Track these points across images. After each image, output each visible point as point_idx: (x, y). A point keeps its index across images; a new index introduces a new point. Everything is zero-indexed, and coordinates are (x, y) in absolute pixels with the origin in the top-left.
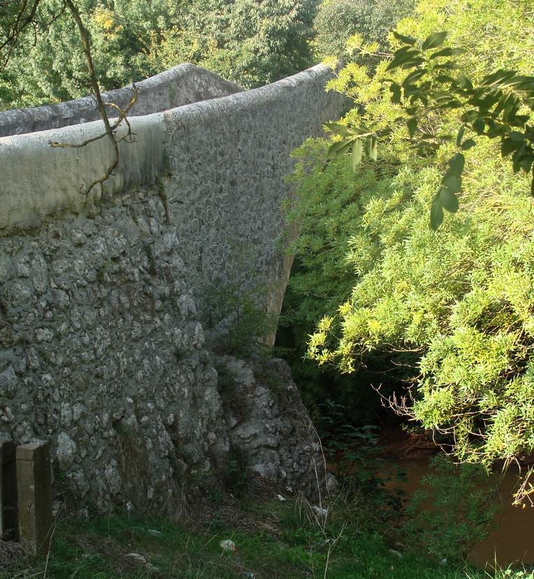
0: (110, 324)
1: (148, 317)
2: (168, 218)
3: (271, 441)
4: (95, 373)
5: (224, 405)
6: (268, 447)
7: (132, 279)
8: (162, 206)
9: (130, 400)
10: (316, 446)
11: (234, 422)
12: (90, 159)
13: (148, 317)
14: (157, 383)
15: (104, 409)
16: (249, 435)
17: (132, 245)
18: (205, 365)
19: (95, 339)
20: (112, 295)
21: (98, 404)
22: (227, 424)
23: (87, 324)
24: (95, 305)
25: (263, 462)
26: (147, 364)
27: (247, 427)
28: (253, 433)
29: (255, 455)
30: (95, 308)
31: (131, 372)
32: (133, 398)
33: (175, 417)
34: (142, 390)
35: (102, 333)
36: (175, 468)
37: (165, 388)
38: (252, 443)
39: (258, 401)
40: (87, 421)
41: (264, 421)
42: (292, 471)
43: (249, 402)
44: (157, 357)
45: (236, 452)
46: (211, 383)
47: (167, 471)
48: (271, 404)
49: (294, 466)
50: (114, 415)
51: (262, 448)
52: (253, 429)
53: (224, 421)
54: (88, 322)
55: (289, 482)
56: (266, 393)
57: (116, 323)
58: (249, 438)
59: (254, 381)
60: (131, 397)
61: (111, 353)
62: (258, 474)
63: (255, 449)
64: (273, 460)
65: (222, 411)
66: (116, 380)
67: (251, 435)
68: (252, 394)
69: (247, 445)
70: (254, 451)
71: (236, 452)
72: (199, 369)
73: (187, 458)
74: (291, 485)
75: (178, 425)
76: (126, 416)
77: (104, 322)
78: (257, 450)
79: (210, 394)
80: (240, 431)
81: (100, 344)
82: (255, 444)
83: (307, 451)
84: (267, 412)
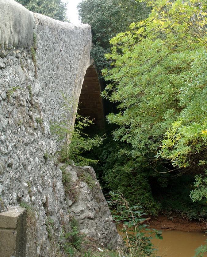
0: (14, 130)
1: (31, 131)
2: (36, 73)
3: (91, 214)
4: (8, 163)
5: (65, 193)
6: (90, 218)
7: (23, 104)
8: (33, 65)
9: (26, 185)
10: (111, 218)
11: (70, 202)
12: (4, 16)
13: (31, 131)
14: (37, 175)
15: (13, 190)
16: (79, 211)
17: (22, 83)
18: (56, 166)
19: (7, 139)
20: (14, 112)
21: (11, 185)
22: (67, 204)
23: (3, 127)
24: (6, 115)
25: (87, 227)
26: (33, 161)
27: (77, 206)
28: (81, 209)
29: (82, 223)
30: (6, 117)
31: (26, 165)
32: (27, 183)
33: (47, 198)
34: (31, 178)
35: (10, 135)
36: (49, 232)
37: (41, 179)
38: (81, 216)
39: (82, 190)
40: (5, 197)
41: (86, 202)
42: (102, 233)
43: (77, 190)
44: (36, 158)
45: (73, 222)
46: (59, 178)
47: (45, 234)
48: (89, 192)
49: (103, 230)
50: (19, 194)
51: (86, 219)
52: (81, 207)
53: (65, 202)
54: (3, 126)
55: (102, 240)
56: (86, 186)
57: (17, 130)
58: (79, 213)
59: (78, 178)
60: (26, 182)
61: (15, 151)
62: (85, 236)
63: (83, 219)
64: (93, 226)
65: (65, 196)
66: (19, 170)
67: (80, 211)
68: (78, 186)
69: (77, 217)
70: (82, 221)
71: (73, 222)
72: (54, 169)
73: (53, 225)
74: (103, 241)
75: (47, 204)
76: (25, 195)
77: (11, 128)
78: (84, 220)
79: (59, 185)
80: (74, 208)
81: (10, 143)
82: (82, 216)
83: (107, 221)
84: (88, 197)
